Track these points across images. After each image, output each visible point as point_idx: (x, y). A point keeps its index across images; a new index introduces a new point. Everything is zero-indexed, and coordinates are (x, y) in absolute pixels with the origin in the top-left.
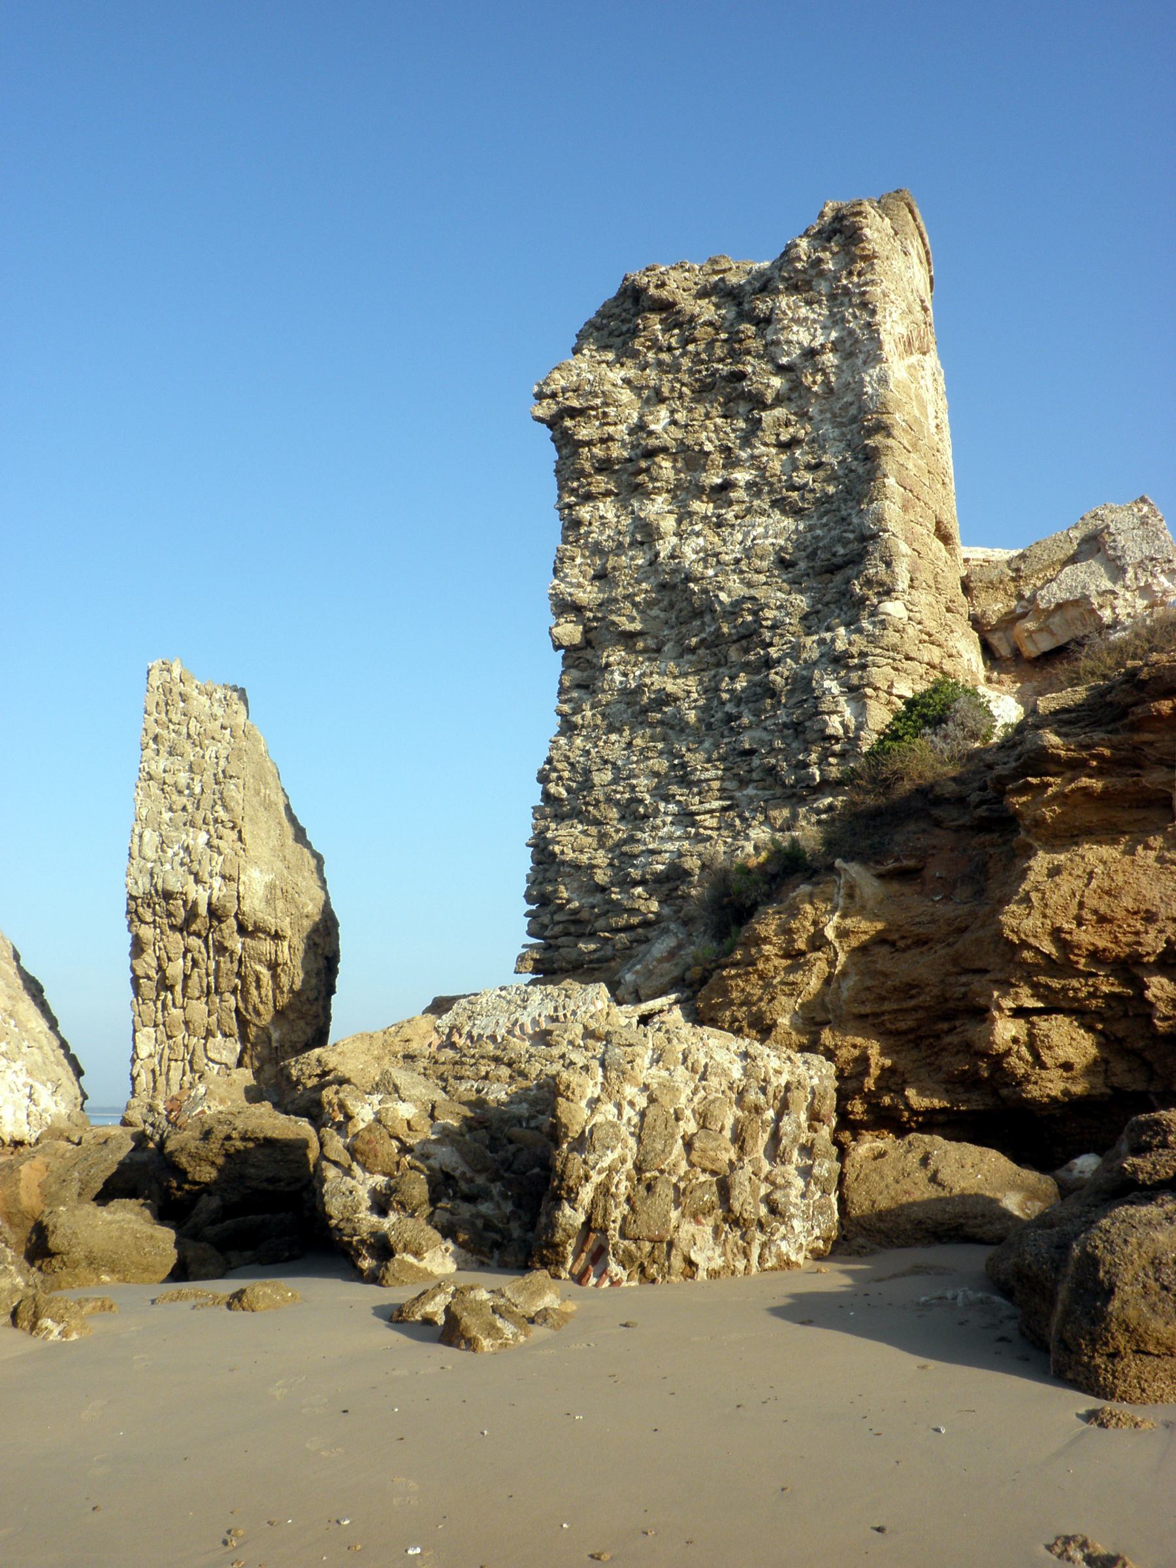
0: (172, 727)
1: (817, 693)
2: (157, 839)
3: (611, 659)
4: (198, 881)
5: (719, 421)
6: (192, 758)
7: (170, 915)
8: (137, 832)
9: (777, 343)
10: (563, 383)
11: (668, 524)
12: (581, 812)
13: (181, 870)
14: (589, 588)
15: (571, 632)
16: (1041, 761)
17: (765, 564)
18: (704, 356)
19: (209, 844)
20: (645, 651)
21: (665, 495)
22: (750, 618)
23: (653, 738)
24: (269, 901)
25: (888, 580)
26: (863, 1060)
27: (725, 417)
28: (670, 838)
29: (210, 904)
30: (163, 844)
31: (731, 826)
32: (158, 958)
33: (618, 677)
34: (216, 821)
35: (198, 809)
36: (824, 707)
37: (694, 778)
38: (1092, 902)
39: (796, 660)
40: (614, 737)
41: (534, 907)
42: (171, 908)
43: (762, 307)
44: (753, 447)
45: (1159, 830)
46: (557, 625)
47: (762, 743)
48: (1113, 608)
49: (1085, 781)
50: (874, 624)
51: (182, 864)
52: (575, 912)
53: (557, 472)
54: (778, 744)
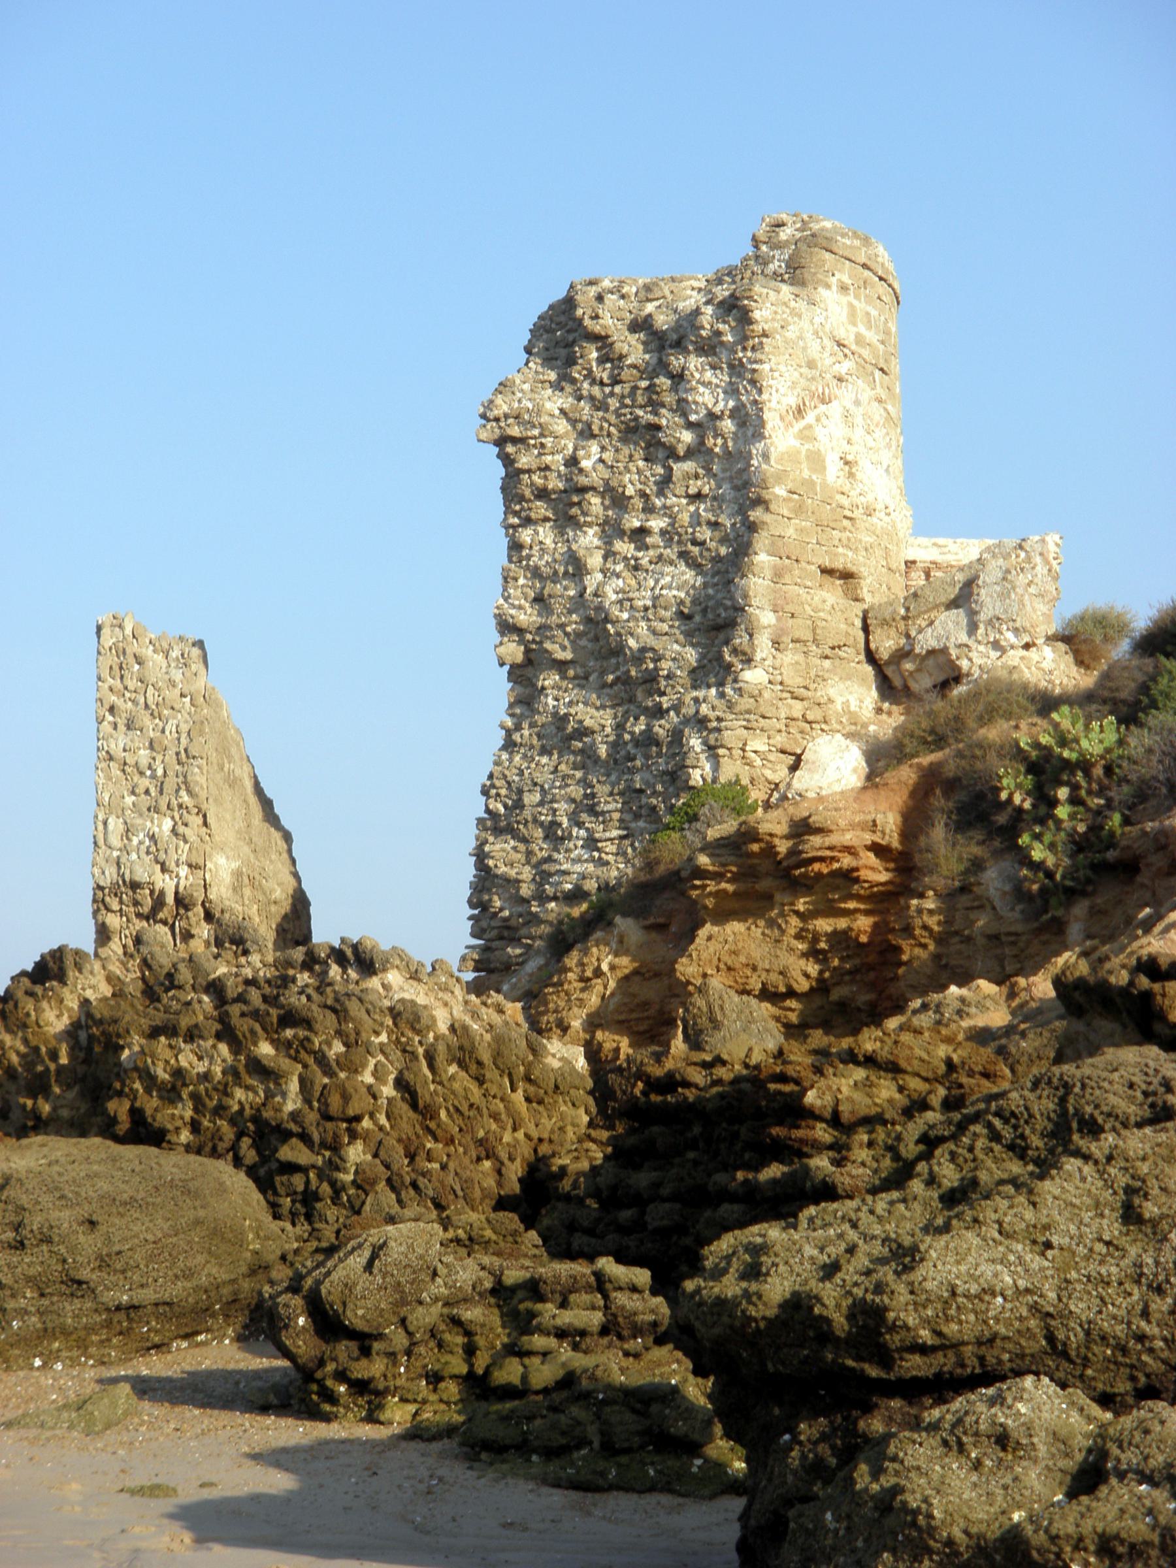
0: (128, 695)
1: (685, 749)
2: (121, 827)
3: (547, 683)
4: (164, 869)
5: (641, 463)
6: (152, 734)
7: (136, 903)
8: (100, 817)
9: (686, 401)
10: (505, 408)
11: (595, 561)
12: (513, 829)
13: (147, 859)
14: (529, 611)
15: (514, 651)
16: (700, 873)
17: (668, 614)
18: (628, 401)
19: (174, 831)
20: (576, 677)
21: (596, 528)
22: (651, 666)
23: (575, 767)
24: (236, 888)
25: (749, 651)
26: (617, 1050)
27: (646, 460)
28: (579, 860)
29: (176, 893)
30: (128, 832)
31: (625, 854)
32: (124, 946)
33: (551, 702)
34: (180, 806)
35: (161, 793)
36: (688, 762)
37: (598, 809)
38: (726, 958)
39: (678, 714)
40: (545, 760)
41: (476, 912)
42: (138, 897)
43: (676, 362)
44: (666, 497)
45: (762, 916)
46: (501, 644)
47: (647, 783)
48: (970, 660)
49: (724, 885)
50: (734, 689)
51: (148, 853)
52: (506, 920)
53: (504, 489)
54: (659, 788)
